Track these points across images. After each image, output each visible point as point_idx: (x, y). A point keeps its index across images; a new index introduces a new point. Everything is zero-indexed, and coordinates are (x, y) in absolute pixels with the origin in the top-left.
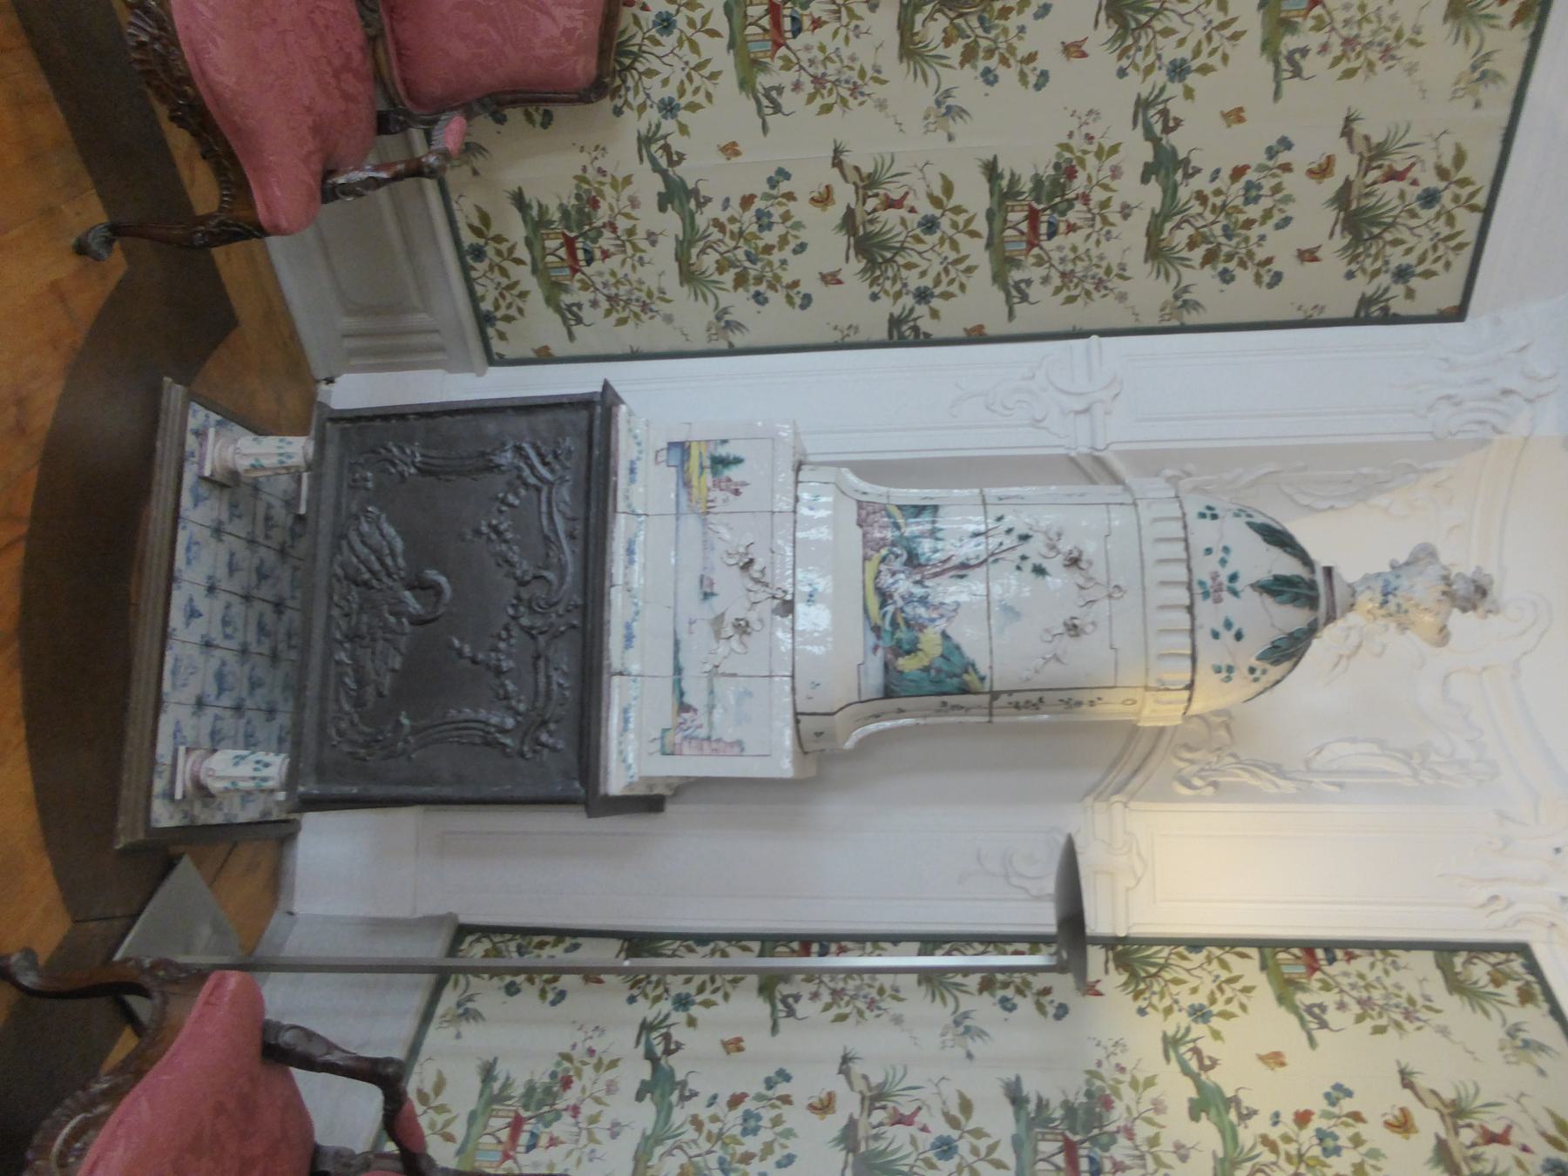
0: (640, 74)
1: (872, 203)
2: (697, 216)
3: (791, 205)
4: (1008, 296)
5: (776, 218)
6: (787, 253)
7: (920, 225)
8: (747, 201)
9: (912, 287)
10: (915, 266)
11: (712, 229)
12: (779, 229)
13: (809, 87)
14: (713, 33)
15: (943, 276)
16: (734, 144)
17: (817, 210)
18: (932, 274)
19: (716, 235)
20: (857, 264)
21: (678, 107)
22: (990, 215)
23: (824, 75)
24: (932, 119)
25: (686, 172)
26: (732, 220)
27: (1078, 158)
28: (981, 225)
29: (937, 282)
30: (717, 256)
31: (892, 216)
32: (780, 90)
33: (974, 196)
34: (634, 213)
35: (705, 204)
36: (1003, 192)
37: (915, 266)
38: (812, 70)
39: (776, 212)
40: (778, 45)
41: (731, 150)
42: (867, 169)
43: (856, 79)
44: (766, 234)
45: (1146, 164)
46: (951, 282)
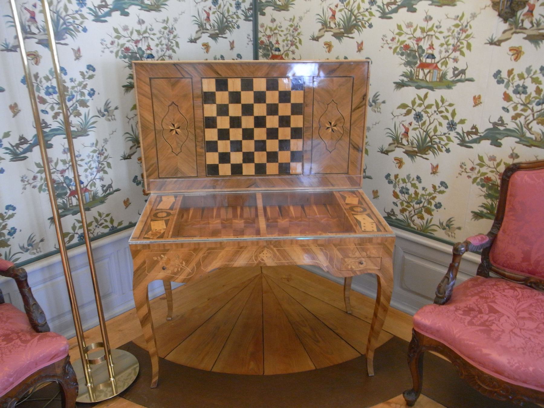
0: (434, 135)
1: (404, 142)
2: (508, 127)
3: (515, 72)
4: (460, 81)
5: (521, 83)
6: (420, 186)
7: (418, 122)
8: (507, 98)
9: (446, 131)
10: (436, 127)
11: (517, 121)
12: (528, 82)
13: (457, 54)
14: (426, 96)
15: (443, 114)
16: (474, 98)
17: (523, 58)
18: (441, 120)
19: (522, 119)
20: (430, 155)
21: (452, 121)
22: (418, 87)
23: (453, 45)
24: (376, 109)
25: (483, 127)
26: (515, 108)
27: (401, 44)
28: (422, 92)
29: (446, 118)
30: (535, 122)
31: (412, 134)
32: (455, 69)
33: (410, 94)
34: (498, 160)
35: (502, 121)
36: (410, 80)
37: (436, 127)
38: (450, 51)
39: (517, 81)
40: (437, 66)
41: (477, 101)
42: (390, 140)
43: (458, 29)
44: (529, 91)
45: (408, 11)
46: (447, 110)
